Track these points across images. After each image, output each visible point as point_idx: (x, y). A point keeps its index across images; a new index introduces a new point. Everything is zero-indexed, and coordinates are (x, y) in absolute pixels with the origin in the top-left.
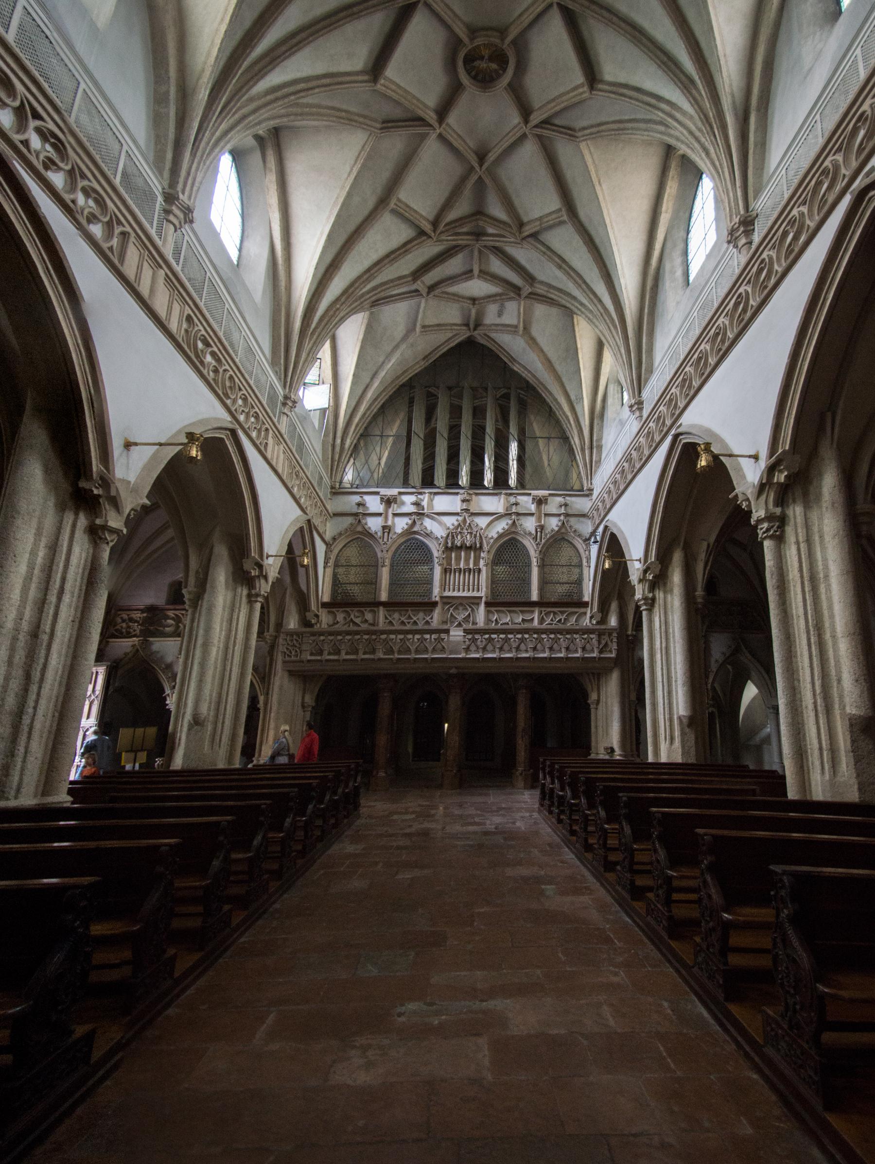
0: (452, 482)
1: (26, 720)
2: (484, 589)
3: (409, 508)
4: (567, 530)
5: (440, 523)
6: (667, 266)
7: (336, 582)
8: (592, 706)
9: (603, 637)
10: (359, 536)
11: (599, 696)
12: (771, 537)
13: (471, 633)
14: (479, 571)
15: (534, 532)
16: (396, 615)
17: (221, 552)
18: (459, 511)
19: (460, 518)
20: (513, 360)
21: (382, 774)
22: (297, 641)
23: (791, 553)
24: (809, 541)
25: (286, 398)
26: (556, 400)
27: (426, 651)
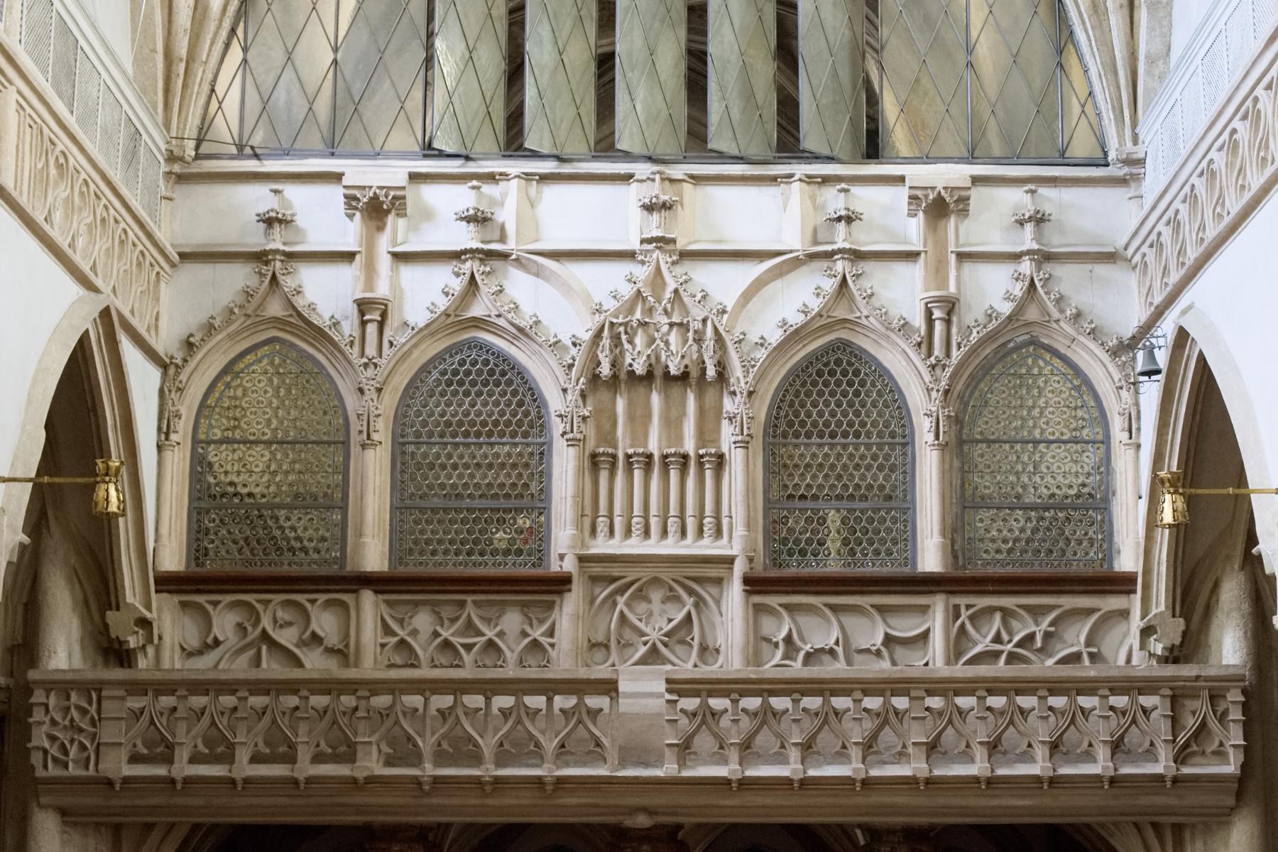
2: (740, 531)
5: (566, 289)
7: (207, 499)
14: (720, 461)
15: (919, 321)
16: (423, 621)
18: (635, 245)
19: (642, 272)
22: (84, 712)
27: (537, 754)
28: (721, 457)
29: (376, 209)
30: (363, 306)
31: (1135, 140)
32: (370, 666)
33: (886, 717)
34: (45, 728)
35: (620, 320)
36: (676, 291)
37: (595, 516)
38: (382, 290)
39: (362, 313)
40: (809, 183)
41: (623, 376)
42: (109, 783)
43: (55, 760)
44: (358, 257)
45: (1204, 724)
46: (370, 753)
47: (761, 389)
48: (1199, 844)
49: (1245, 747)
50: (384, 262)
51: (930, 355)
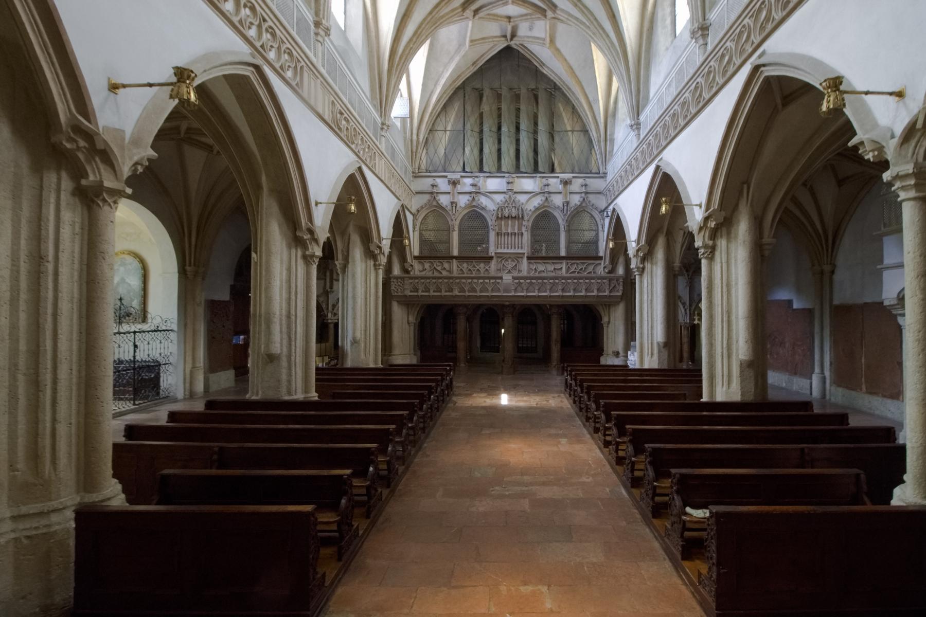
1: (293, 358)
3: (469, 189)
5: (492, 200)
6: (660, 14)
7: (423, 242)
10: (437, 211)
12: (706, 258)
14: (522, 234)
15: (561, 206)
16: (465, 265)
17: (356, 239)
20: (542, 64)
21: (462, 365)
23: (717, 268)
24: (728, 262)
25: (383, 124)
26: (578, 99)
27: (487, 291)
29: (454, 183)
30: (452, 203)
32: (455, 274)
33: (531, 284)
38: (456, 200)
50: (456, 194)
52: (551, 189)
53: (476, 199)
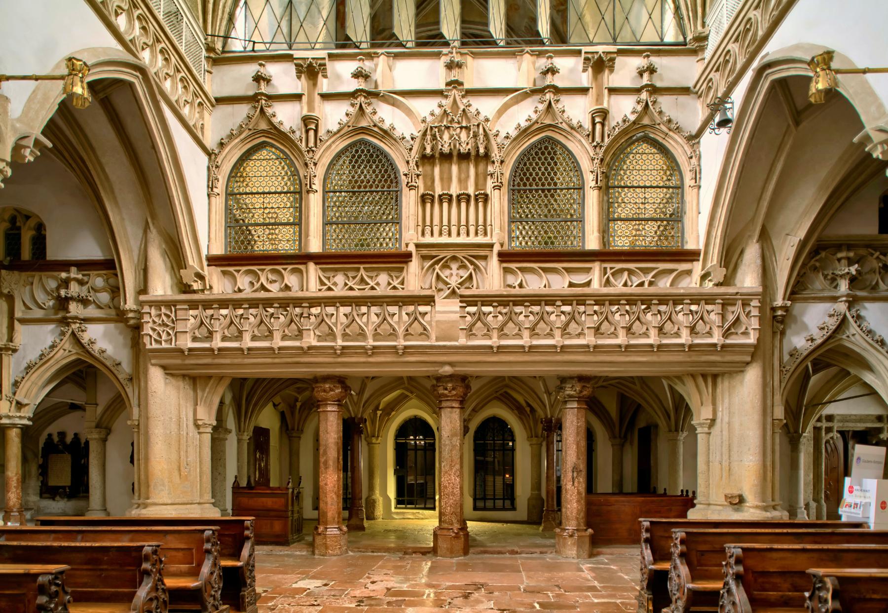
0: (429, 39)
2: (497, 230)
4: (653, 120)
5: (408, 112)
8: (699, 430)
9: (730, 309)
11: (715, 412)
13: (474, 304)
14: (486, 198)
15: (587, 125)
18: (442, 86)
19: (447, 103)
21: (332, 531)
22: (168, 316)
28: (487, 195)
30: (306, 120)
31: (703, 25)
34: (150, 325)
35: (436, 125)
36: (464, 110)
37: (424, 226)
39: (306, 126)
40: (532, 55)
41: (437, 155)
42: (181, 351)
43: (155, 340)
44: (304, 97)
45: (738, 319)
46: (309, 335)
47: (507, 161)
48: (726, 383)
49: (759, 329)
51: (593, 141)
52: (559, 81)
53: (368, 110)
